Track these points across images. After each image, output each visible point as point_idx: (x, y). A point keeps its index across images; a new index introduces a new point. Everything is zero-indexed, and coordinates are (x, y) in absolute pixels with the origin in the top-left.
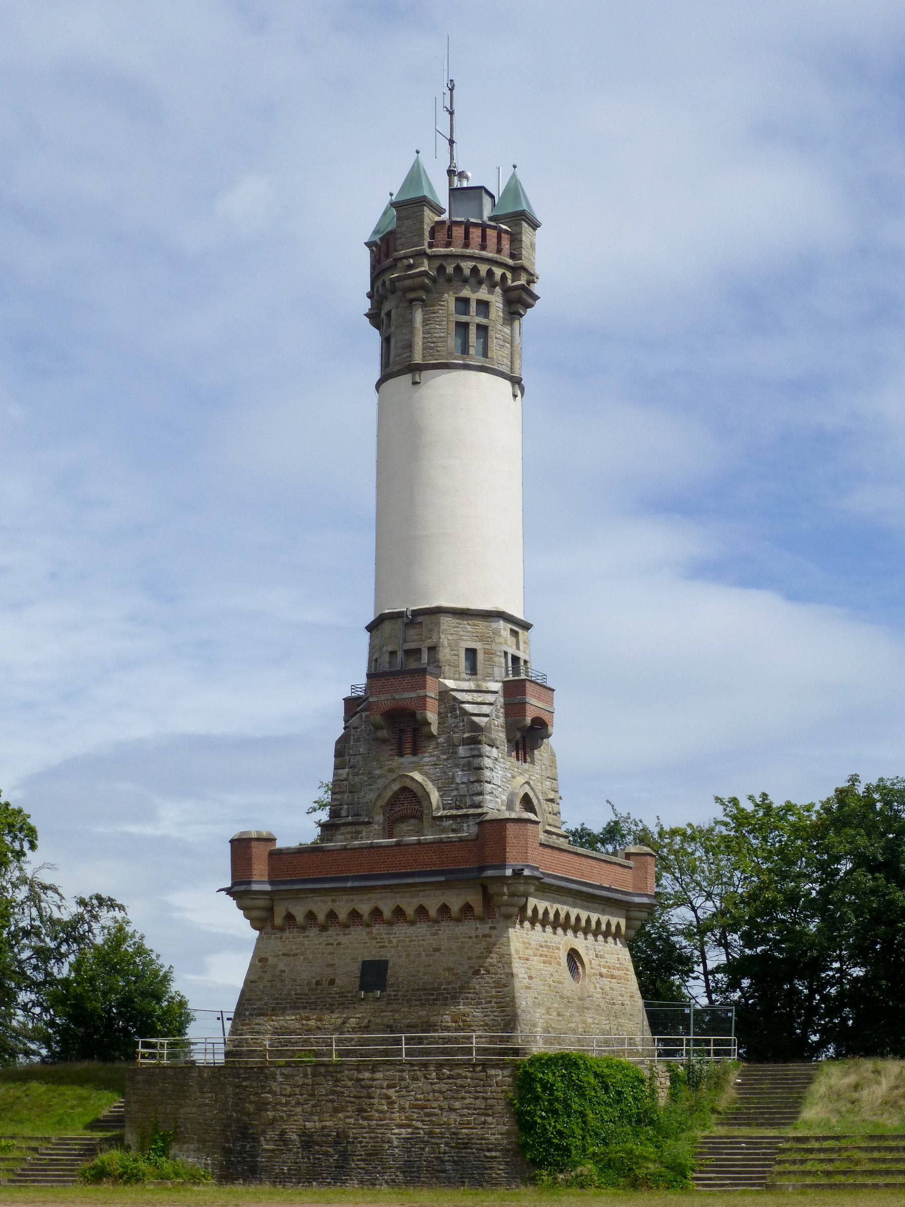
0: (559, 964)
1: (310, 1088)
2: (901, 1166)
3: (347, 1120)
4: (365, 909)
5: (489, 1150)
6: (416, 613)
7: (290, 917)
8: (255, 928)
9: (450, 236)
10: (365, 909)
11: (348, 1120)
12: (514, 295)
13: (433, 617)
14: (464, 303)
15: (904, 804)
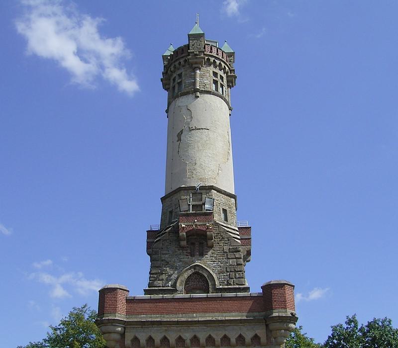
6: (202, 188)
12: (230, 79)
14: (215, 74)
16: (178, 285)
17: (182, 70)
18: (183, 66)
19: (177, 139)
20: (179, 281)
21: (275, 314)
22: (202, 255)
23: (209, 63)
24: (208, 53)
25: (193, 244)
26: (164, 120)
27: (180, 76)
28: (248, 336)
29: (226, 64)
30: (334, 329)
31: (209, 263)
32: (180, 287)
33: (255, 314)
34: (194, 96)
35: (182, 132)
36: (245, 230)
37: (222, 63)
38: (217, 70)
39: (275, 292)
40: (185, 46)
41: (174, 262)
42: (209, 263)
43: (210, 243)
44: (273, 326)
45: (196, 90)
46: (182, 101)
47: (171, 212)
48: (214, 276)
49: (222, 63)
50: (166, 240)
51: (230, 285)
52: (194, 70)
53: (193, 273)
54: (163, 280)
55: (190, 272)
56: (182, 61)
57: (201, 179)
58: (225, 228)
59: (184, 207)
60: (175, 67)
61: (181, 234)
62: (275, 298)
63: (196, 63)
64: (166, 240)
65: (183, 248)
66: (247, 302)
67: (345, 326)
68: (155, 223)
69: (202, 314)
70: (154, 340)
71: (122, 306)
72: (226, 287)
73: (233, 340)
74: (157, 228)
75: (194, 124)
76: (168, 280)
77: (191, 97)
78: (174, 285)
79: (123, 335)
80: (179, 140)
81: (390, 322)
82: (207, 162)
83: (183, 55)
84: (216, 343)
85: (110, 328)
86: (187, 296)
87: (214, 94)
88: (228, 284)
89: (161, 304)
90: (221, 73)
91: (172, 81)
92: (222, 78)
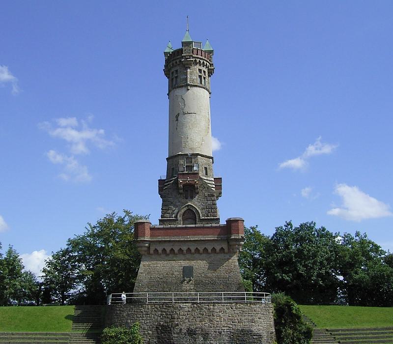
0: (60, 309)
1: (181, 314)
2: (392, 339)
3: (206, 324)
4: (185, 248)
5: (254, 336)
6: (193, 155)
7: (156, 251)
8: (280, 235)
9: (197, 52)
10: (185, 248)
11: (206, 325)
12: (210, 71)
13: (172, 155)
14: (200, 71)
15: (1, 276)
16: (178, 217)
17: (178, 68)
18: (179, 65)
19: (175, 119)
20: (179, 214)
21: (233, 237)
22: (192, 198)
23: (196, 63)
24: (196, 56)
25: (187, 191)
26: (166, 101)
27: (177, 71)
28: (218, 248)
29: (207, 61)
30: (277, 229)
31: (196, 203)
32: (179, 218)
33: (222, 236)
34: (186, 89)
35: (179, 114)
36: (218, 180)
37: (205, 62)
38: (201, 68)
39: (233, 224)
40: (180, 49)
41: (176, 202)
42: (196, 203)
43: (196, 191)
44: (232, 243)
45: (188, 85)
46: (178, 92)
47: (173, 169)
48: (199, 211)
49: (205, 62)
50: (170, 188)
51: (209, 216)
52: (186, 69)
53: (187, 210)
54: (169, 213)
55: (185, 209)
56: (178, 61)
57: (191, 149)
58: (206, 181)
59: (181, 169)
60: (173, 64)
61: (179, 186)
62: (233, 228)
63: (187, 64)
64: (170, 188)
65: (181, 194)
66: (218, 229)
67: (284, 228)
68: (163, 175)
69: (193, 237)
70: (165, 250)
71: (148, 232)
72: (206, 218)
73: (210, 251)
74: (165, 178)
75: (186, 111)
76: (172, 214)
77: (184, 89)
78: (176, 217)
79: (149, 248)
80: (177, 120)
81: (315, 224)
82: (195, 137)
83: (179, 57)
84: (200, 252)
85: (142, 244)
86: (184, 226)
87: (199, 87)
88: (207, 216)
89: (169, 231)
90: (204, 69)
91: (171, 74)
92: (204, 72)
